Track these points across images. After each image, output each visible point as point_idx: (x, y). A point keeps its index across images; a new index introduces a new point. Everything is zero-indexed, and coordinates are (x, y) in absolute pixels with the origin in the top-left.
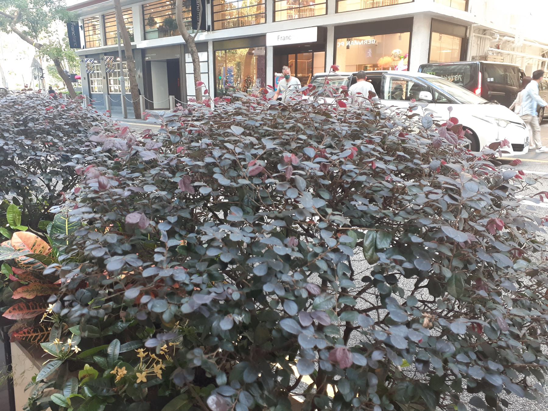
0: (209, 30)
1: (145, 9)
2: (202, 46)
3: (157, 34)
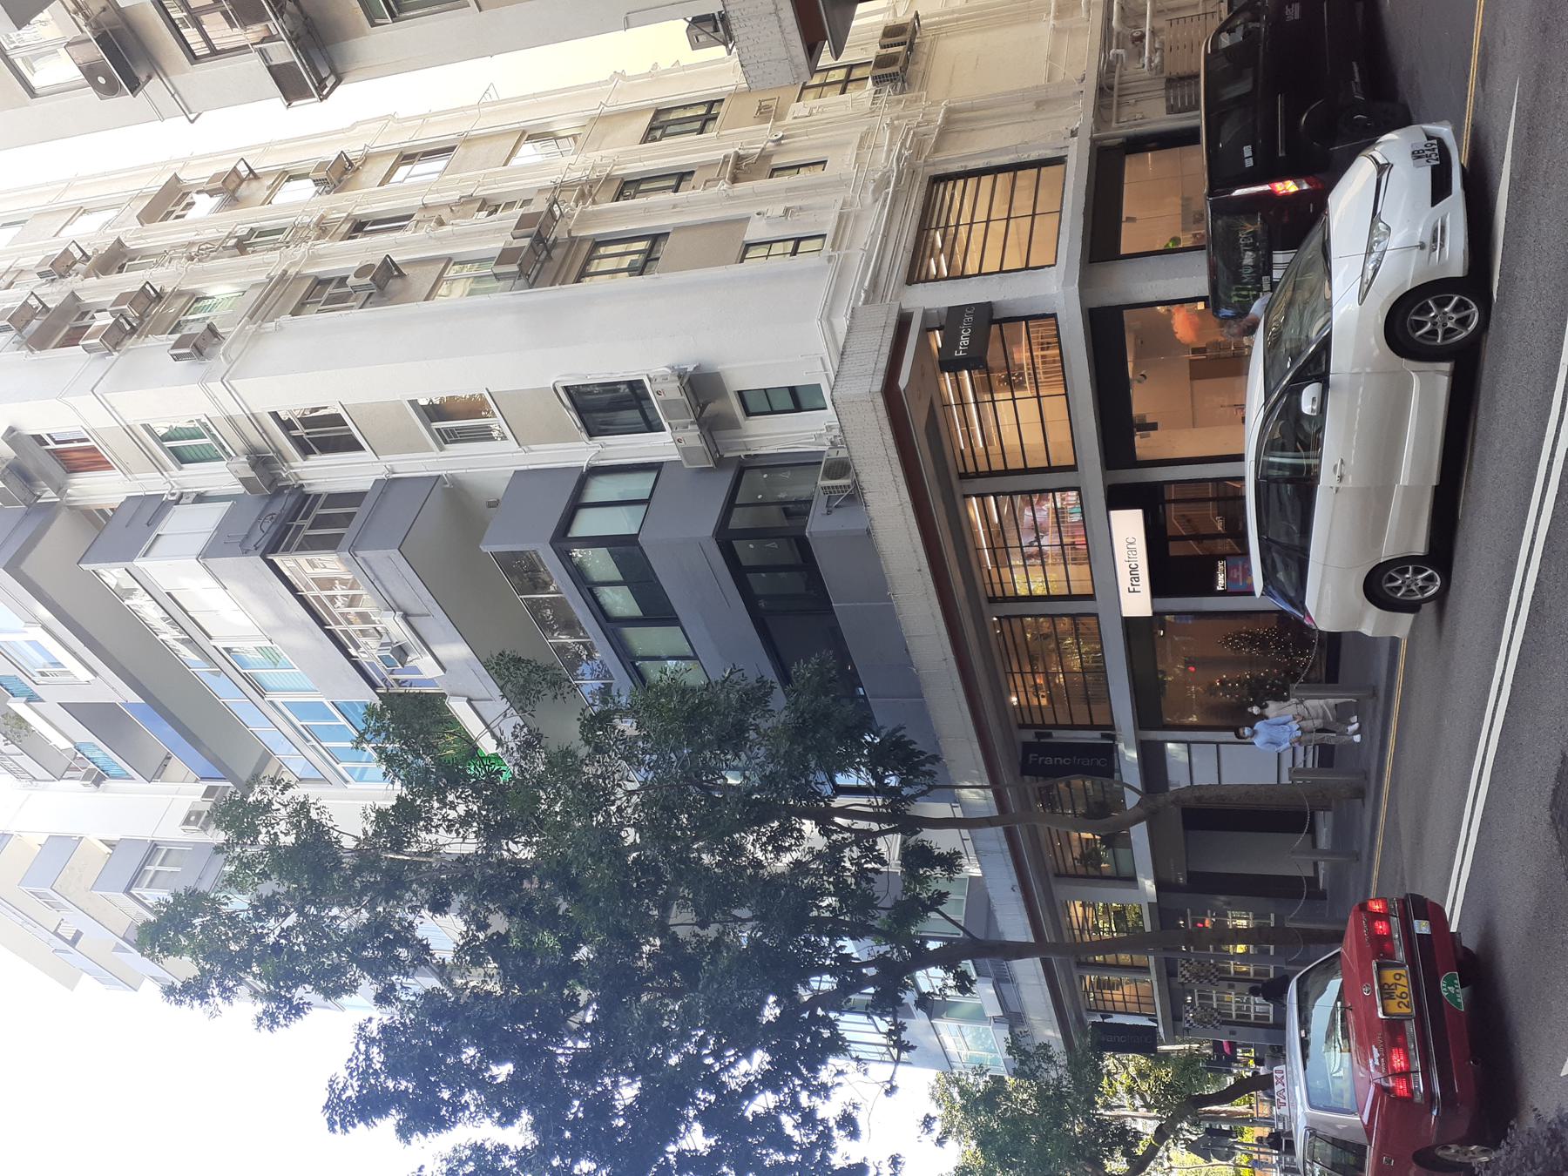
0: (1113, 738)
1: (999, 593)
2: (1152, 759)
3: (1121, 852)
